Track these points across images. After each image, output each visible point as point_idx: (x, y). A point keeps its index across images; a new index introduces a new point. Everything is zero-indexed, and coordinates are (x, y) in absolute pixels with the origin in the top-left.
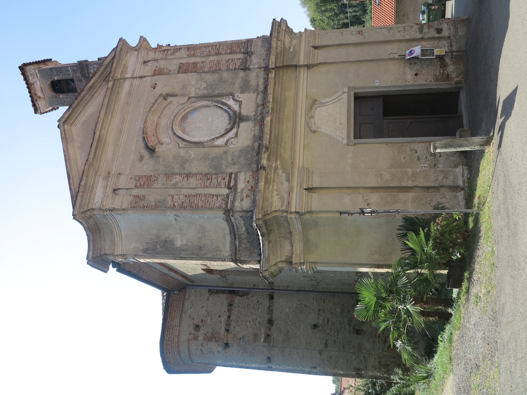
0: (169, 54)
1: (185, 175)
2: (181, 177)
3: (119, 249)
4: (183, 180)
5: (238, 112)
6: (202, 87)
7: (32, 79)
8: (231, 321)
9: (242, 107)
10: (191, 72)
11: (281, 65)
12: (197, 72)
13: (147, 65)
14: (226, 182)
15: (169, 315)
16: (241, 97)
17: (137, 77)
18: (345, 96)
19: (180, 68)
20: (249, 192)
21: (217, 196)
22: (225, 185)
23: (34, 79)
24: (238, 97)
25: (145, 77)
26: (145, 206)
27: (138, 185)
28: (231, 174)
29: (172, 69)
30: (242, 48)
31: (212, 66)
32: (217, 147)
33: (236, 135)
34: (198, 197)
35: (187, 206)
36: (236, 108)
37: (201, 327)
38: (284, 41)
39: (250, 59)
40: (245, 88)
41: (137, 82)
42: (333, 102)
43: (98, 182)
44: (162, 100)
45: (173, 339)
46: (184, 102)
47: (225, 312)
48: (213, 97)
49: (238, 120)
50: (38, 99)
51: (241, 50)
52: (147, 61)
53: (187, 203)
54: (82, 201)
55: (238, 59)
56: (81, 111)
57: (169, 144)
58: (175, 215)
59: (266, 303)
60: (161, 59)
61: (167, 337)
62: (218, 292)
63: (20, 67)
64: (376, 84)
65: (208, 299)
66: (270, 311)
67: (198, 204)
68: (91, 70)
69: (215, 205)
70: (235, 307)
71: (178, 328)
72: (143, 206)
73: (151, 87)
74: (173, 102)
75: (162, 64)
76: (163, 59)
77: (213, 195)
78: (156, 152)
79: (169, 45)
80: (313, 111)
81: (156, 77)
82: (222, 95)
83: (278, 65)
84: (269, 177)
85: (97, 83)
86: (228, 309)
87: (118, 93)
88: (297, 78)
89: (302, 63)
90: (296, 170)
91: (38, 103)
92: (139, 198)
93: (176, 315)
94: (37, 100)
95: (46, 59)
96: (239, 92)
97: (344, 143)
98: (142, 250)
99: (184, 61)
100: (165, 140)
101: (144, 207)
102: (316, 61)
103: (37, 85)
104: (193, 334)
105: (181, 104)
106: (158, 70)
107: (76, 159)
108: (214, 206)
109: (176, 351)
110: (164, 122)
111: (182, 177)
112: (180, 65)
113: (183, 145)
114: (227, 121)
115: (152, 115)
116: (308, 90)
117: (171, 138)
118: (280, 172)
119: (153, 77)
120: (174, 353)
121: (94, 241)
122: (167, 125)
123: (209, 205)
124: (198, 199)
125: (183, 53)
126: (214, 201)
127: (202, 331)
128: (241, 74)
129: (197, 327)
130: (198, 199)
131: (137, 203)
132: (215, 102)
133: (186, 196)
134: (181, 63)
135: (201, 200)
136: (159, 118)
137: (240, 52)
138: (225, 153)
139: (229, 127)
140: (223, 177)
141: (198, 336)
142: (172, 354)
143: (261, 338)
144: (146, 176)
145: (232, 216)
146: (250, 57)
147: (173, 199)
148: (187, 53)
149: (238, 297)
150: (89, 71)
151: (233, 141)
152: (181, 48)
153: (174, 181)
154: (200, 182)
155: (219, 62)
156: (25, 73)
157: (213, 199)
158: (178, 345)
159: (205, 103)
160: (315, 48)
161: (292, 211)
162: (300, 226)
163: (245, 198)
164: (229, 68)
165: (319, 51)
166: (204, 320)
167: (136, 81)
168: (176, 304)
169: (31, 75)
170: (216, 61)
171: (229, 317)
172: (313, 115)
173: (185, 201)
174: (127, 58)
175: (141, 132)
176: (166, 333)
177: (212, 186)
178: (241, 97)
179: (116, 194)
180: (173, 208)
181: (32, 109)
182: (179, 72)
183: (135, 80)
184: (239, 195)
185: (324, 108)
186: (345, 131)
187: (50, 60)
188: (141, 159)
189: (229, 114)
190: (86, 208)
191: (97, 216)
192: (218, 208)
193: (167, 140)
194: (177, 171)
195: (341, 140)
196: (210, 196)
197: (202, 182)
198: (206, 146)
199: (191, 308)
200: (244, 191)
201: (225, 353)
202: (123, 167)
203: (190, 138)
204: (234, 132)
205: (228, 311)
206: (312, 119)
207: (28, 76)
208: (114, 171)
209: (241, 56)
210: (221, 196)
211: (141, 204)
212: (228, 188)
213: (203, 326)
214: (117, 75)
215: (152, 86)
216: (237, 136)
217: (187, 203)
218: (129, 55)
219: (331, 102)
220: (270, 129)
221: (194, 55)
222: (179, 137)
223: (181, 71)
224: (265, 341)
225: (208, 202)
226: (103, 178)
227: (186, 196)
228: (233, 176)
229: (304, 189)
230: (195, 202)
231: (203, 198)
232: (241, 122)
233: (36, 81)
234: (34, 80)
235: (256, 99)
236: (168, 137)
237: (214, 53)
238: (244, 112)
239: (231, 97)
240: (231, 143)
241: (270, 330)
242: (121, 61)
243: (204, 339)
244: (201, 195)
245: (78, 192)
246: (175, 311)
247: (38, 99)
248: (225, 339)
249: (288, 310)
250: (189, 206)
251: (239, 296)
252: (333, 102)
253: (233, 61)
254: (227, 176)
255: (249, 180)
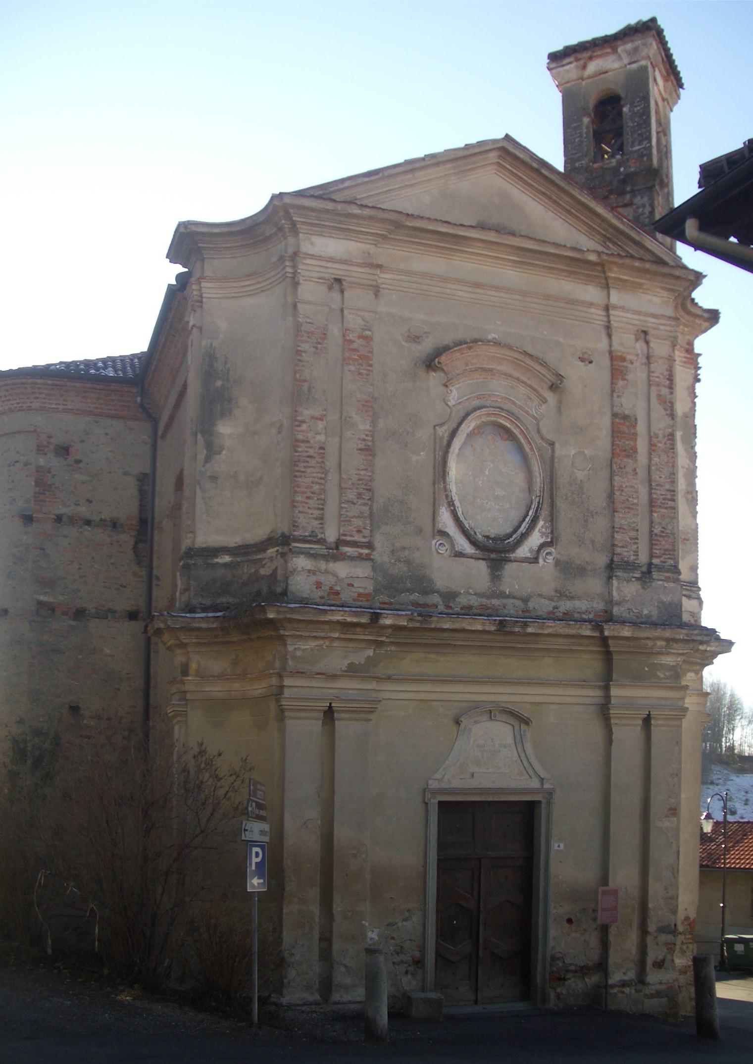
0: (659, 391)
1: (370, 443)
2: (367, 435)
3: (214, 291)
4: (359, 439)
5: (512, 556)
6: (576, 471)
7: (626, 51)
8: (81, 527)
9: (524, 564)
10: (613, 445)
11: (611, 649)
12: (613, 458)
13: (637, 340)
14: (351, 536)
15: (88, 385)
16: (547, 562)
17: (608, 316)
18: (535, 784)
19: (625, 417)
20: (327, 588)
21: (321, 518)
22: (345, 535)
23: (626, 55)
24: (547, 554)
25: (609, 336)
26: (301, 355)
27: (351, 337)
28: (370, 546)
29: (623, 400)
30: (662, 559)
31: (624, 494)
32: (434, 513)
33: (460, 555)
34: (320, 475)
35: (300, 452)
36: (523, 551)
37: (66, 459)
38: (668, 654)
39: (633, 579)
40: (566, 568)
41: (598, 318)
42: (524, 758)
43: (360, 242)
44: (551, 381)
45: (37, 398)
46: (544, 431)
47: (100, 513)
48: (552, 497)
49: (493, 556)
50: (582, 62)
51: (657, 557)
52: (648, 338)
53: (307, 452)
54: (312, 210)
55: (637, 552)
56: (533, 186)
57: (445, 402)
58: (282, 425)
59: (123, 604)
60: (650, 372)
61: (40, 384)
62: (142, 493)
63: (653, 20)
64: (556, 845)
65: (126, 474)
66: (105, 614)
67: (305, 477)
68: (639, 198)
69: (300, 515)
70: (110, 536)
71: (61, 407)
72: (301, 351)
73: (584, 350)
74: (544, 406)
75: (637, 373)
76: (649, 376)
77: (323, 509)
78: (428, 372)
79: (699, 380)
80: (504, 717)
81: (606, 362)
82: (552, 519)
83: (610, 642)
84: (358, 629)
85: (600, 222)
86: (105, 521)
87: (571, 273)
88: (582, 684)
89: (614, 692)
90: (373, 685)
91: (570, 63)
92: (319, 340)
93: (88, 400)
94: (577, 60)
95: (681, 75)
96: (558, 556)
97: (430, 782)
98: (211, 345)
99: (641, 427)
100: (455, 392)
101: (299, 353)
102: (617, 721)
103: (613, 61)
104: (48, 443)
105: (538, 424)
106: (623, 366)
107: (417, 183)
108: (300, 512)
109: (13, 404)
110: (498, 387)
111: (366, 438)
112: (633, 419)
113: (441, 434)
114: (493, 532)
115: (515, 358)
116: (552, 706)
117: (459, 407)
118: (370, 652)
119: (607, 354)
120: (8, 400)
121: (231, 234)
122: (489, 395)
123: (302, 502)
124: (315, 475)
125: (661, 423)
126: (310, 511)
127: (55, 463)
128: (602, 560)
129: (64, 450)
130: (315, 475)
131: (308, 337)
132: (539, 502)
133: (323, 448)
134: (636, 419)
135: (313, 483)
136: (508, 376)
137: (652, 556)
138: (420, 531)
139: (479, 537)
140: (364, 528)
141: (46, 454)
142: (5, 396)
143: (45, 594)
144: (372, 352)
145: (277, 551)
146: (637, 579)
147: (317, 419)
148: (660, 433)
149: (132, 541)
150: (636, 192)
151: (444, 548)
152: (673, 419)
153: (357, 418)
154: (354, 479)
155: (632, 509)
156: (640, 35)
157: (315, 508)
158: (24, 410)
159: (538, 480)
160: (647, 721)
161: (284, 678)
162: (257, 693)
163: (313, 579)
164: (617, 532)
165: (639, 728)
166: (81, 465)
167: (600, 315)
168: (113, 400)
169: (636, 50)
170: (635, 501)
171: (88, 523)
172: (496, 718)
173: (311, 447)
174: (658, 290)
175: (476, 335)
176: (50, 382)
177: (343, 505)
178: (547, 562)
179: (330, 288)
180: (296, 421)
181: (558, 47)
182: (615, 415)
183: (605, 314)
184: (323, 565)
185: (510, 740)
186: (457, 784)
187: (681, 85)
188: (415, 339)
189: (509, 536)
190: (298, 219)
191: (283, 243)
192: (295, 522)
193: (454, 396)
194: (381, 424)
195: (438, 776)
196: (322, 502)
197: (353, 484)
198: (436, 486)
199: (107, 434)
200: (330, 577)
201: (13, 517)
202: (394, 297)
203: (457, 451)
204: (465, 550)
205: (101, 520)
206: (488, 715)
207: (632, 41)
208: (384, 278)
209: (643, 558)
210: (321, 526)
211: (305, 346)
212: (338, 540)
213: (68, 465)
214: (615, 269)
215: (586, 353)
216: (456, 556)
217: (307, 452)
218: (665, 294)
219: (522, 755)
220: (463, 630)
221: (652, 447)
222: (460, 424)
223: (617, 420)
224: (40, 603)
225: (308, 498)
226: (369, 254)
227: (323, 448)
228: (365, 551)
229: (330, 704)
230: (309, 470)
231: (316, 487)
232: (489, 564)
233: (620, 58)
234: (624, 56)
235: (540, 595)
236: (463, 397)
237: (655, 496)
238: (509, 569)
239: (549, 540)
240: (441, 544)
241: (64, 614)
242: (649, 276)
243: (39, 469)
244: (323, 481)
245: (334, 201)
246: (98, 399)
247: (582, 62)
248: (41, 516)
249: (108, 651)
250: (299, 456)
251: (136, 543)
252: (524, 758)
253: (633, 541)
254: (364, 537)
255: (355, 586)
